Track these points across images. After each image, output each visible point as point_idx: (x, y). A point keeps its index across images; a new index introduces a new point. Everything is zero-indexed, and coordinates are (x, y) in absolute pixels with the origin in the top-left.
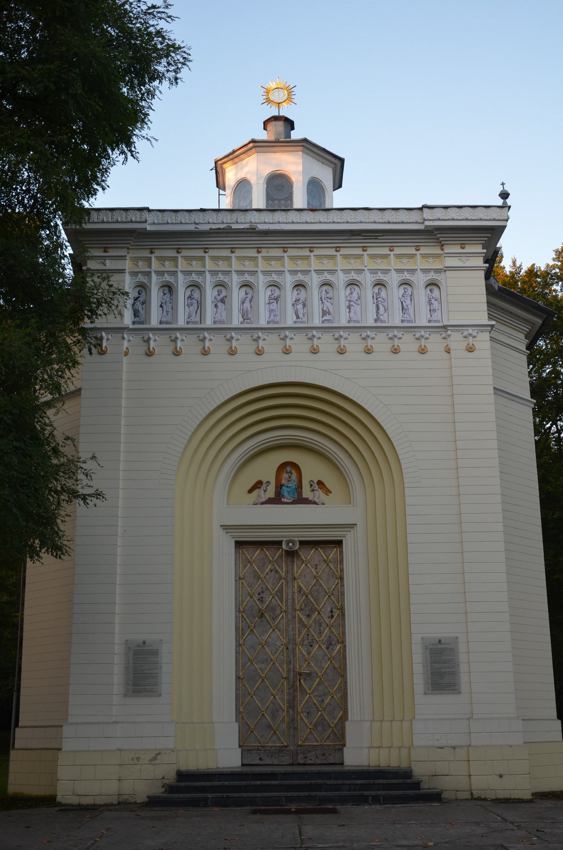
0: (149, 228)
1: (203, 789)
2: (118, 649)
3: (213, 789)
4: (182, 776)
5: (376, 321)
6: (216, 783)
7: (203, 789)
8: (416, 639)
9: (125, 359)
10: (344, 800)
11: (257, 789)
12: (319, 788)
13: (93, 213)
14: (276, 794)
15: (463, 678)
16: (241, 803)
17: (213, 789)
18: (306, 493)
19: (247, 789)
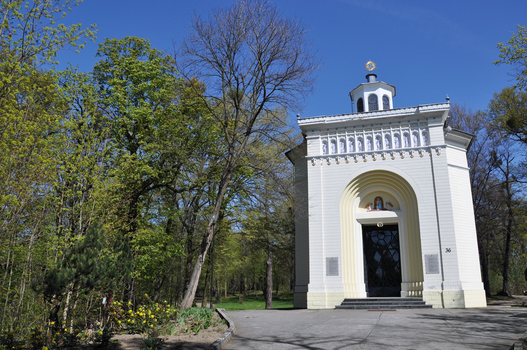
0: (326, 122)
1: (353, 304)
2: (324, 260)
3: (356, 304)
4: (346, 300)
5: (405, 146)
6: (357, 302)
7: (353, 304)
8: (423, 255)
9: (321, 166)
10: (399, 307)
11: (370, 304)
12: (391, 304)
13: (396, 232)
14: (424, 261)
15: (339, 273)
16: (365, 308)
17: (356, 304)
18: (385, 206)
19: (367, 304)
